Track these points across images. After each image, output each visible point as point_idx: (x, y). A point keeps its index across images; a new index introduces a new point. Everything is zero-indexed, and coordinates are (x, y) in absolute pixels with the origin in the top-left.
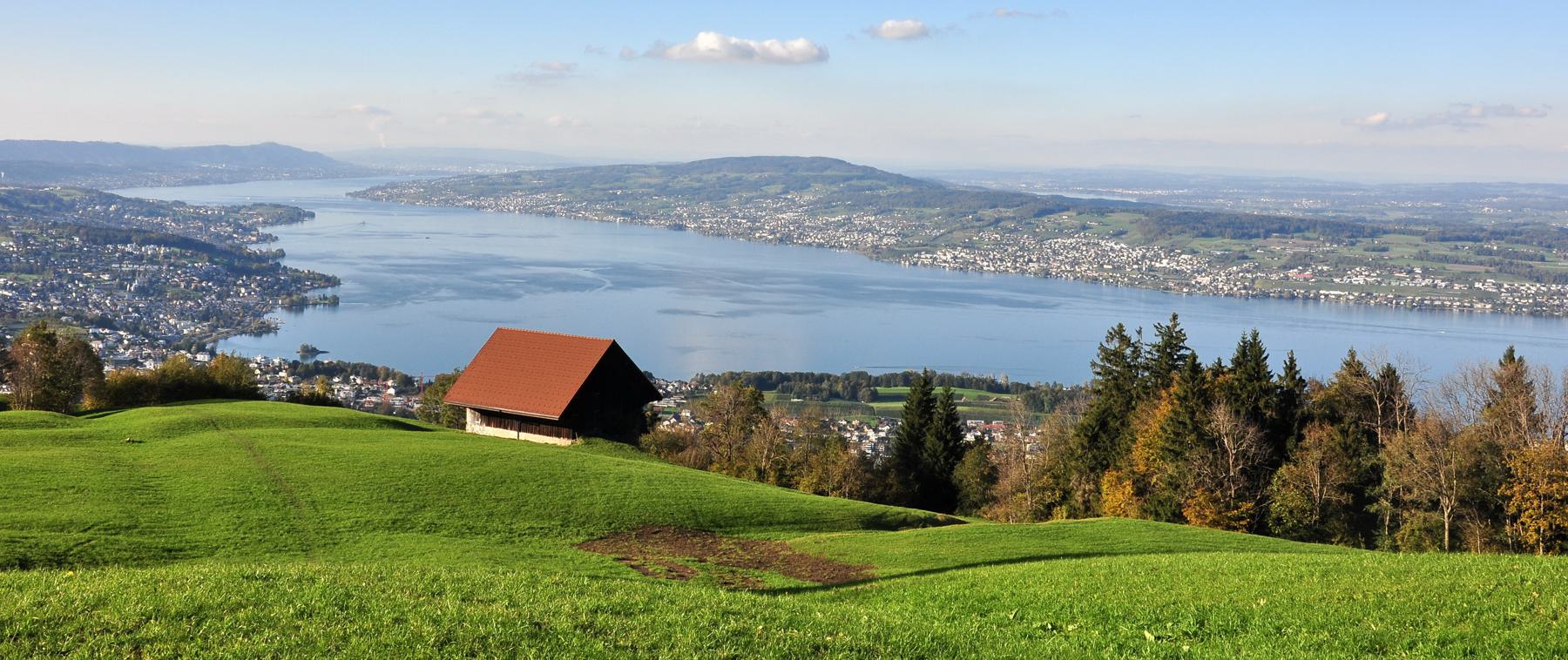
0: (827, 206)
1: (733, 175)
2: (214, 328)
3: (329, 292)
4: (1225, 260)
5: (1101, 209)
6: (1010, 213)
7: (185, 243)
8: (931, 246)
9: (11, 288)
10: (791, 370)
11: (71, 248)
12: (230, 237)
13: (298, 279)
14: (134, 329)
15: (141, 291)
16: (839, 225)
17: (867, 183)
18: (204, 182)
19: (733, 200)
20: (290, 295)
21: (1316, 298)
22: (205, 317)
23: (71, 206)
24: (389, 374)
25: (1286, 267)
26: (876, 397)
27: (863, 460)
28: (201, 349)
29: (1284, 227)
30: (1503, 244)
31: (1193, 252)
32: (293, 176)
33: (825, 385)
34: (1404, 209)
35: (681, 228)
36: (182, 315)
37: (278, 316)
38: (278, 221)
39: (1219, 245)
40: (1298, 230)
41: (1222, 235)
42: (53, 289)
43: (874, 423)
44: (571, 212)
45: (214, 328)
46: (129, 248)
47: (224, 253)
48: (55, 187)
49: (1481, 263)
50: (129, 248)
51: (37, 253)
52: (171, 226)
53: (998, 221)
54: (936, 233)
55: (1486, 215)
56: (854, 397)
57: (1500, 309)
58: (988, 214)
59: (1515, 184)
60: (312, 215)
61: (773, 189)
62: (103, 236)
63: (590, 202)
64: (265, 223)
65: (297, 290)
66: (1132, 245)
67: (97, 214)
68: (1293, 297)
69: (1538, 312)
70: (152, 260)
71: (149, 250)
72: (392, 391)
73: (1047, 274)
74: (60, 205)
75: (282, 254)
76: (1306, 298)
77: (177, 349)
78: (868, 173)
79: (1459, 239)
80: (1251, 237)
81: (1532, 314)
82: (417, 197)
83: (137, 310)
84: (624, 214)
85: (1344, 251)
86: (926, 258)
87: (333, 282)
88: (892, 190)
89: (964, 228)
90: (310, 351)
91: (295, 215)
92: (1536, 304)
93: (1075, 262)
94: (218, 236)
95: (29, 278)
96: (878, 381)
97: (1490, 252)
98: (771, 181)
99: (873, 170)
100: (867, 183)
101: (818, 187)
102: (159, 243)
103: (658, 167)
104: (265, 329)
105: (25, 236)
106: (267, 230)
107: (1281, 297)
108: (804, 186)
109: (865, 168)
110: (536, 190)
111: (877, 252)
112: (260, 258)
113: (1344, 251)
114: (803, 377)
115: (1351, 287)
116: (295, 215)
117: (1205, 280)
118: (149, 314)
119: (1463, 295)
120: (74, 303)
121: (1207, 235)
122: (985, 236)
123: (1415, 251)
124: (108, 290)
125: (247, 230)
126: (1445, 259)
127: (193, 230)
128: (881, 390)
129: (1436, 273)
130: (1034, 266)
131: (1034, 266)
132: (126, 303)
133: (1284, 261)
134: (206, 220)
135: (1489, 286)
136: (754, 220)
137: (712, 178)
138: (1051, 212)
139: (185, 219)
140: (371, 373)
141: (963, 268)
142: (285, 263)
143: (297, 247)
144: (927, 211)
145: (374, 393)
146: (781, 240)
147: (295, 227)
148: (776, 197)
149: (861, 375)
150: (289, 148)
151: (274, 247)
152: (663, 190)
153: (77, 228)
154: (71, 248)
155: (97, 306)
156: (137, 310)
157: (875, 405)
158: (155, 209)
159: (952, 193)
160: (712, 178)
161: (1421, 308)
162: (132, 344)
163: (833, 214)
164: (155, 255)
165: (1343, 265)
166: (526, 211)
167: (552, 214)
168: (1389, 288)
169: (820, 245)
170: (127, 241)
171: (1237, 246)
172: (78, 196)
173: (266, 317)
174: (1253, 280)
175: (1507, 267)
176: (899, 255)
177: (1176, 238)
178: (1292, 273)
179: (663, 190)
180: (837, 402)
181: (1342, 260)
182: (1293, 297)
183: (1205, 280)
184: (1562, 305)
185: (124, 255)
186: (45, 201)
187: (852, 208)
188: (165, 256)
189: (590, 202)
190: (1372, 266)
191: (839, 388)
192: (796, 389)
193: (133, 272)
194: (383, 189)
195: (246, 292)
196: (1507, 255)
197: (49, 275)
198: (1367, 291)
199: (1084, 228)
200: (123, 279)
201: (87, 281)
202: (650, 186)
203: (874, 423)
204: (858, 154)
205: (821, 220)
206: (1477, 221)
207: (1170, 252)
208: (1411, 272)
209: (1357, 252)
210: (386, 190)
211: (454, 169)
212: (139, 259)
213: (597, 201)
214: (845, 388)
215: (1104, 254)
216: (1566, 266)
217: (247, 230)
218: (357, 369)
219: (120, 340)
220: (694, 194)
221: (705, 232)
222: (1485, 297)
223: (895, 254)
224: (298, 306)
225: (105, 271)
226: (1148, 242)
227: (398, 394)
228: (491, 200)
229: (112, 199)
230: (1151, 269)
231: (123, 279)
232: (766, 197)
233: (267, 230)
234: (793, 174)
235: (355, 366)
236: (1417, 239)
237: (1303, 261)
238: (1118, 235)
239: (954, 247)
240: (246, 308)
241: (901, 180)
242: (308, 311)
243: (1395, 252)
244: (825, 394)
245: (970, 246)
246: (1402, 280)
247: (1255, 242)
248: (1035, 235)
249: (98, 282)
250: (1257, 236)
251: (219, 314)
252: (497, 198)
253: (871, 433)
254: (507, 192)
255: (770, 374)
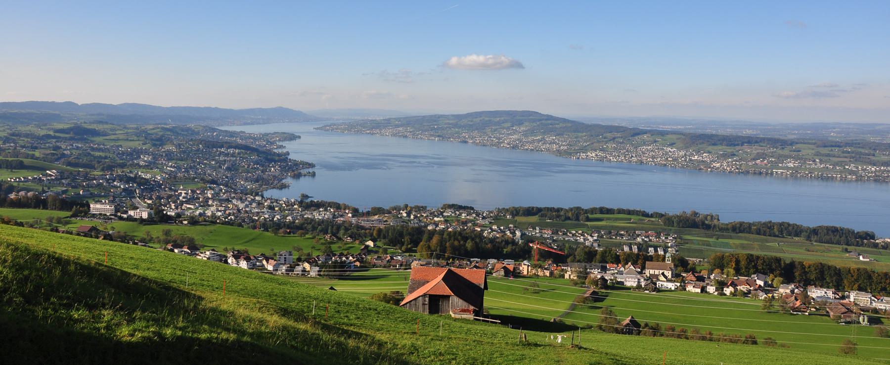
0: (532, 132)
1: (487, 119)
2: (261, 186)
3: (311, 170)
4: (725, 156)
5: (662, 133)
6: (619, 135)
7: (246, 148)
8: (584, 150)
9: (174, 167)
10: (542, 206)
11: (198, 150)
12: (265, 146)
13: (296, 164)
14: (226, 186)
15: (228, 169)
16: (539, 141)
17: (549, 122)
18: (252, 124)
19: (488, 130)
20: (293, 171)
21: (772, 174)
22: (257, 181)
23: (198, 133)
24: (346, 207)
25: (754, 159)
26: (588, 220)
27: (529, 260)
28: (257, 194)
29: (750, 141)
30: (853, 149)
31: (709, 152)
32: (290, 121)
33: (562, 213)
34: (795, 134)
35: (466, 142)
36: (246, 180)
37: (288, 181)
38: (285, 139)
39: (721, 149)
40: (756, 142)
41: (721, 144)
42: (191, 168)
43: (590, 232)
44: (414, 136)
45: (261, 186)
46: (222, 150)
47: (264, 153)
48: (191, 125)
49: (846, 157)
50: (222, 150)
51: (184, 152)
52: (239, 141)
53: (614, 138)
54: (585, 144)
55: (833, 136)
56: (577, 219)
57: (860, 179)
58: (609, 135)
59: (876, 125)
60: (299, 137)
61: (508, 125)
62: (212, 145)
63: (423, 131)
64: (280, 140)
65: (297, 169)
66: (679, 149)
67: (209, 136)
68: (760, 173)
69: (878, 179)
70: (233, 155)
71: (231, 151)
72: (350, 215)
73: (642, 162)
74: (194, 133)
75: (288, 153)
76: (767, 174)
77: (246, 194)
78: (549, 117)
79: (832, 146)
80: (735, 145)
81: (875, 181)
82: (345, 129)
83: (227, 177)
84: (439, 136)
85: (781, 152)
86: (583, 155)
87: (311, 165)
88: (561, 125)
89: (598, 142)
90: (305, 196)
91: (292, 137)
92: (877, 176)
93: (653, 157)
94: (260, 146)
95: (181, 163)
96: (586, 211)
97: (849, 152)
98: (505, 121)
99: (551, 116)
100: (549, 122)
101: (527, 124)
102: (236, 147)
103: (453, 116)
104: (284, 187)
105: (179, 145)
106: (281, 143)
107: (755, 173)
108: (520, 123)
109: (548, 116)
110: (397, 126)
111: (559, 153)
112: (279, 155)
113: (781, 152)
114: (548, 209)
115: (788, 168)
116: (292, 137)
117: (718, 165)
118: (232, 179)
119: (841, 172)
120: (200, 174)
121: (715, 144)
122: (609, 145)
123: (813, 152)
124: (214, 168)
125: (272, 143)
126: (828, 155)
127: (249, 143)
128: (590, 216)
129: (826, 162)
130: (634, 159)
131: (634, 159)
132: (222, 174)
133: (753, 156)
134: (254, 139)
135: (852, 167)
136: (499, 139)
137: (478, 120)
138: (638, 134)
139: (246, 139)
140: (338, 207)
141: (601, 160)
142: (289, 157)
143: (296, 151)
144: (580, 134)
145: (342, 216)
146: (513, 148)
147: (293, 142)
148: (508, 129)
149: (578, 208)
150: (287, 109)
151: (284, 151)
152: (456, 125)
153: (201, 142)
154: (198, 150)
155: (210, 175)
156: (227, 177)
157: (588, 223)
158: (232, 134)
159: (590, 126)
160: (478, 120)
161: (822, 178)
162: (226, 192)
163: (536, 136)
164: (234, 153)
165: (781, 158)
166: (394, 135)
167: (406, 137)
168: (806, 169)
169: (532, 150)
170: (221, 147)
171: (730, 150)
172: (201, 128)
173: (284, 181)
174: (741, 165)
175: (858, 158)
176: (570, 154)
177: (700, 146)
178: (758, 161)
179: (456, 125)
180: (570, 222)
181: (780, 156)
182: (760, 173)
183: (718, 165)
184: (888, 176)
185: (221, 153)
186: (187, 131)
187: (544, 133)
188: (239, 154)
189: (423, 131)
190: (796, 158)
191: (570, 215)
192: (548, 215)
193: (225, 161)
194: (330, 126)
195: (274, 170)
196: (857, 153)
197: (190, 162)
198: (796, 169)
199: (655, 142)
200: (220, 164)
201: (205, 164)
202: (449, 124)
203: (590, 232)
204: (544, 109)
205: (530, 139)
206: (830, 139)
207: (698, 152)
208: (814, 161)
209: (786, 152)
210: (330, 126)
211: (359, 118)
212: (227, 155)
213: (426, 131)
214: (573, 215)
215: (667, 153)
216: (885, 158)
217: (272, 143)
218: (331, 205)
219: (221, 190)
220: (471, 127)
221: (477, 144)
222: (851, 172)
223: (568, 153)
224: (297, 176)
225: (213, 160)
226: (686, 148)
227: (353, 216)
228: (378, 131)
229: (214, 130)
230: (691, 160)
231: (220, 164)
232: (504, 128)
233: (281, 143)
234: (515, 118)
235: (329, 203)
236: (812, 146)
237: (763, 156)
238: (672, 145)
239: (596, 151)
240: (275, 177)
241: (565, 121)
242: (302, 179)
243: (804, 152)
244: (563, 218)
245: (602, 150)
246: (810, 165)
247: (738, 148)
248: (633, 145)
249: (210, 165)
250: (738, 145)
251: (263, 179)
252: (381, 130)
253: (589, 237)
254: (385, 127)
255: (533, 208)
